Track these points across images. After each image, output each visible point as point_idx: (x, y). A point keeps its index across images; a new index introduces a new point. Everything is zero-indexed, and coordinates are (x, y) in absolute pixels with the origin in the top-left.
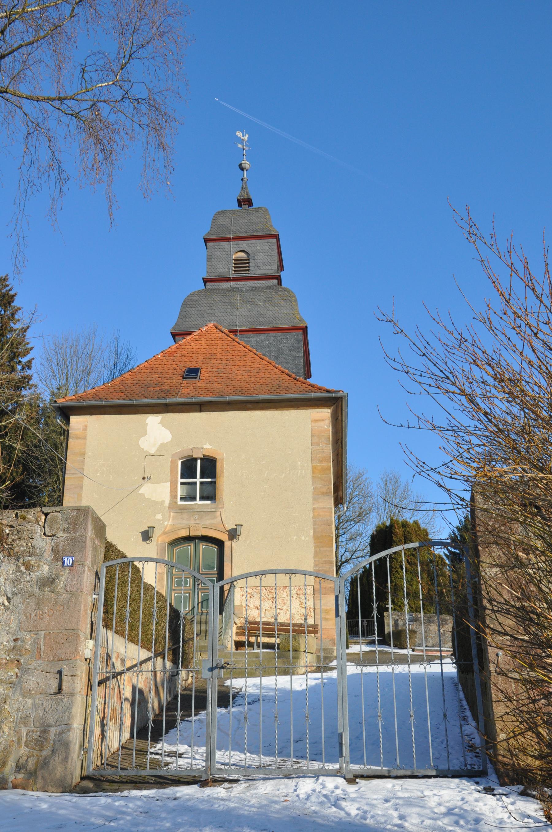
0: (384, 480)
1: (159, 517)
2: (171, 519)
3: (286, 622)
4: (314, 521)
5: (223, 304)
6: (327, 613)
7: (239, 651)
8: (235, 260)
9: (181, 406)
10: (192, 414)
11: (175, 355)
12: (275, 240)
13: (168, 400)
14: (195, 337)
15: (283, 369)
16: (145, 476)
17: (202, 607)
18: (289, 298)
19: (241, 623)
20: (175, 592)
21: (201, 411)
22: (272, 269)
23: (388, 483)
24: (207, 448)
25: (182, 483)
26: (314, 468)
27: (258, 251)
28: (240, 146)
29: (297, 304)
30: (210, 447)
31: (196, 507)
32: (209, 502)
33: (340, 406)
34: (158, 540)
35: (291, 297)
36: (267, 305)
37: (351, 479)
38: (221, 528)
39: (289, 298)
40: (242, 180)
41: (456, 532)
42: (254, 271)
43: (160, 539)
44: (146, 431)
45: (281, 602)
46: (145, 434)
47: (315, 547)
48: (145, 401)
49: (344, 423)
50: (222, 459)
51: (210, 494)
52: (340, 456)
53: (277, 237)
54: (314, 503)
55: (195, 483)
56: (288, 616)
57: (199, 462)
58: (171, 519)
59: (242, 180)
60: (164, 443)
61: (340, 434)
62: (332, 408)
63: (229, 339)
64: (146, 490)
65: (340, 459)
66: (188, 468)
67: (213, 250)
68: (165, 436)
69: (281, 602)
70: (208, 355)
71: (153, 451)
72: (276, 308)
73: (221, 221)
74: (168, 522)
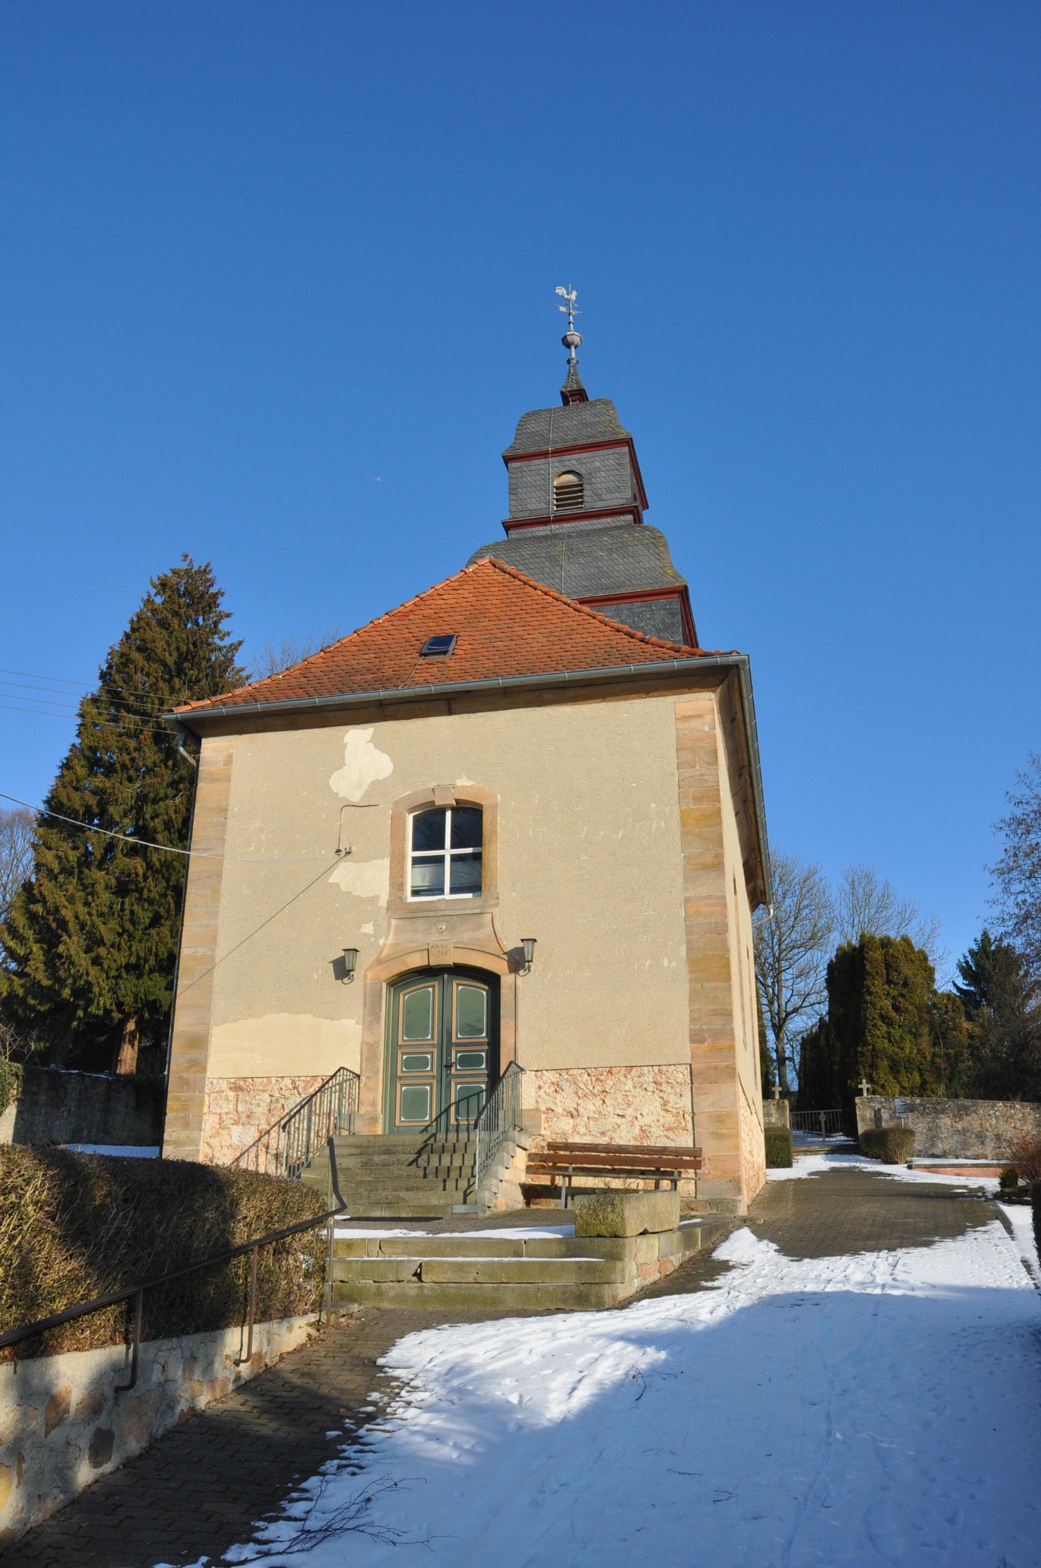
0: (850, 880)
1: (368, 928)
2: (392, 933)
3: (633, 1143)
4: (687, 926)
5: (537, 560)
6: (722, 1122)
7: (533, 1207)
8: (557, 488)
9: (411, 705)
10: (432, 720)
11: (412, 617)
12: (626, 449)
13: (382, 694)
14: (452, 584)
15: (617, 625)
16: (341, 848)
17: (457, 1113)
18: (653, 541)
19: (536, 1147)
20: (402, 1082)
21: (450, 713)
22: (623, 497)
23: (856, 884)
24: (465, 785)
25: (416, 861)
26: (684, 815)
27: (598, 470)
28: (562, 309)
29: (667, 550)
30: (469, 783)
31: (443, 907)
32: (470, 896)
33: (736, 687)
34: (365, 977)
35: (657, 540)
36: (615, 556)
37: (796, 881)
38: (493, 947)
39: (653, 541)
40: (569, 362)
41: (969, 959)
42: (591, 503)
43: (368, 972)
44: (344, 759)
45: (621, 1101)
46: (344, 765)
47: (691, 981)
48: (338, 699)
49: (748, 727)
50: (495, 807)
51: (471, 877)
52: (750, 804)
53: (628, 442)
54: (686, 889)
55: (440, 860)
56: (637, 1131)
57: (449, 814)
58: (392, 933)
59: (569, 362)
60: (378, 780)
61: (745, 755)
62: (719, 689)
63: (519, 583)
64: (344, 875)
65: (751, 811)
66: (428, 831)
67: (520, 474)
68: (383, 766)
69: (621, 1101)
70: (474, 612)
71: (356, 798)
72: (631, 559)
73: (532, 427)
74: (387, 939)
